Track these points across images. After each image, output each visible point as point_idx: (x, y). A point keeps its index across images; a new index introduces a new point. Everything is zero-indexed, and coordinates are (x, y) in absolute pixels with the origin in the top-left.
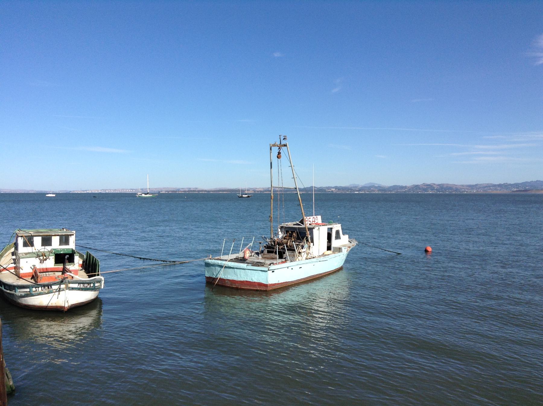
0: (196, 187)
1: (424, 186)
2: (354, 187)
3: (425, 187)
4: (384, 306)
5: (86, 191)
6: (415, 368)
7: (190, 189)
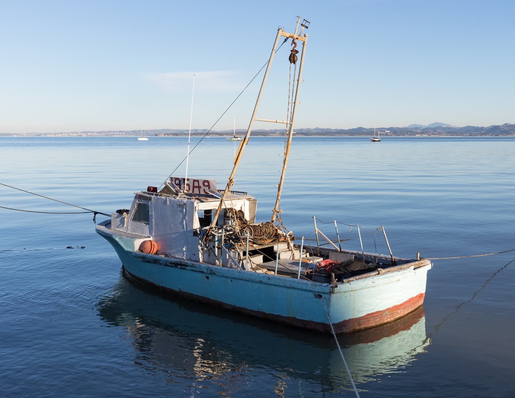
0: (204, 128)
1: (506, 127)
2: (414, 128)
3: (508, 129)
4: (38, 240)
5: (62, 133)
6: (101, 240)
7: (196, 130)
